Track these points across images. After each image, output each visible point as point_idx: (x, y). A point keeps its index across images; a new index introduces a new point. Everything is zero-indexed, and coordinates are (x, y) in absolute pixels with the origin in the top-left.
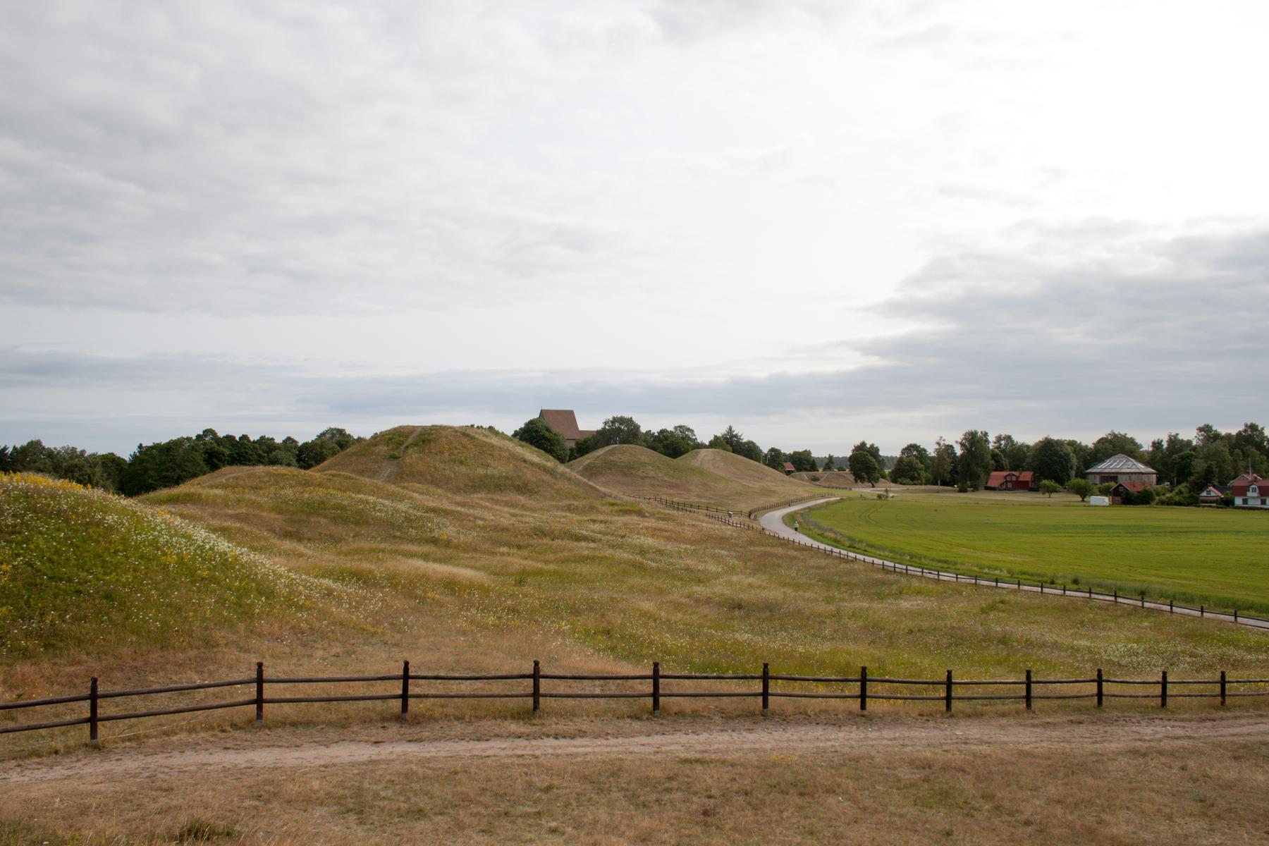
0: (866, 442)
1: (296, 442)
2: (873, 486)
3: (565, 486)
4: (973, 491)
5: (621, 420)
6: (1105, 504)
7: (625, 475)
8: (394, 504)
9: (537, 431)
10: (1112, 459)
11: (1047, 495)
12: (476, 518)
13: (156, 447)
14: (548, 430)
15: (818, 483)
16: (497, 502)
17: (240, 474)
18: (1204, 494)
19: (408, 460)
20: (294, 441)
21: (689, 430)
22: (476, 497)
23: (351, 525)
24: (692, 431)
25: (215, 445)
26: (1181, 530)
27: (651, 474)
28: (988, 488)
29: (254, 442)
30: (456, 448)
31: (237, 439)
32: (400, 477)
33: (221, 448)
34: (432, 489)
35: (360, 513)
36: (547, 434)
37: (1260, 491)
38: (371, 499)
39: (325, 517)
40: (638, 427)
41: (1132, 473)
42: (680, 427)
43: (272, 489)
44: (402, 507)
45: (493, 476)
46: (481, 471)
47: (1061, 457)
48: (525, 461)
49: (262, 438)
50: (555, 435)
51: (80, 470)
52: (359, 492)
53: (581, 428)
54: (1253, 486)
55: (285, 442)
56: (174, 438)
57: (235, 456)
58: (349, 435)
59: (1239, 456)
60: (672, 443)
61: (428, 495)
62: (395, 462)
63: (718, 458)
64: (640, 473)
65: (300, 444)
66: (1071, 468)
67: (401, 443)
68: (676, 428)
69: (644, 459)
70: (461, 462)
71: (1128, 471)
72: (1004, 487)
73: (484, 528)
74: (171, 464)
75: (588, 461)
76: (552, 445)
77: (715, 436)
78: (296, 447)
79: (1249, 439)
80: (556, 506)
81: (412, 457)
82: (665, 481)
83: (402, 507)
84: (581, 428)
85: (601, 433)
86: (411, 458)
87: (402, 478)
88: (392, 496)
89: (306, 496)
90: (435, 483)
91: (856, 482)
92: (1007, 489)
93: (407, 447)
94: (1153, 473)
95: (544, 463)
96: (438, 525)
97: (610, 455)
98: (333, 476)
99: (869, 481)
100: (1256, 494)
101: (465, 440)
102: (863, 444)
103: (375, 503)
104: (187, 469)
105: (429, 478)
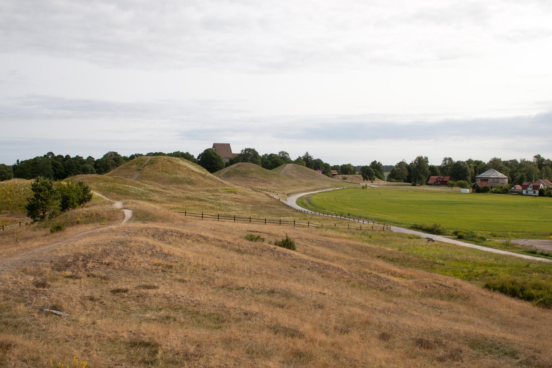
0: (423, 156)
1: (94, 159)
2: (372, 182)
3: (209, 182)
4: (420, 185)
5: (249, 150)
6: (467, 192)
7: (243, 176)
8: (138, 189)
9: (209, 155)
10: (487, 171)
11: (450, 188)
12: (167, 193)
13: (26, 162)
14: (215, 154)
15: (346, 180)
16: (179, 188)
17: (83, 178)
18: (513, 188)
19: (145, 171)
20: (92, 158)
21: (286, 153)
22: (171, 186)
23: (123, 195)
24: (288, 154)
25: (54, 160)
26: (459, 203)
27: (255, 176)
28: (427, 184)
29: (73, 158)
30: (164, 166)
31: (64, 157)
32: (141, 178)
33: (57, 162)
34: (153, 183)
35: (126, 191)
36: (214, 156)
37: (533, 188)
38: (130, 187)
39: (115, 192)
40: (193, 156)
41: (494, 178)
42: (282, 152)
43: (95, 183)
44: (141, 189)
45: (178, 178)
46: (174, 176)
47: (463, 169)
48: (193, 171)
49: (77, 156)
50: (218, 156)
51: (5, 174)
52: (126, 184)
53: (233, 152)
54: (531, 185)
55: (88, 158)
56: (35, 157)
57: (67, 166)
58: (119, 155)
59: (543, 171)
60: (276, 161)
61: (151, 185)
62: (140, 172)
63: (294, 168)
64: (250, 176)
65: (95, 160)
66: (468, 175)
67: (142, 164)
68: (280, 153)
69: (253, 169)
70: (166, 172)
71: (493, 177)
72: (436, 184)
73: (168, 197)
74: (37, 170)
75: (227, 170)
76: (216, 161)
77: (299, 157)
78: (94, 161)
79: (540, 162)
80: (202, 189)
81: (147, 169)
82: (261, 179)
83: (141, 189)
84: (233, 152)
85: (240, 155)
86: (146, 170)
87: (142, 178)
88: (138, 185)
89: (108, 185)
90: (155, 180)
91: (364, 180)
92: (438, 185)
93: (144, 166)
94: (507, 178)
95: (201, 172)
96: (153, 195)
97: (238, 167)
98: (116, 178)
99: (370, 180)
100: (531, 189)
101: (168, 163)
102: (375, 162)
103: (131, 188)
104: (44, 172)
105: (153, 178)
